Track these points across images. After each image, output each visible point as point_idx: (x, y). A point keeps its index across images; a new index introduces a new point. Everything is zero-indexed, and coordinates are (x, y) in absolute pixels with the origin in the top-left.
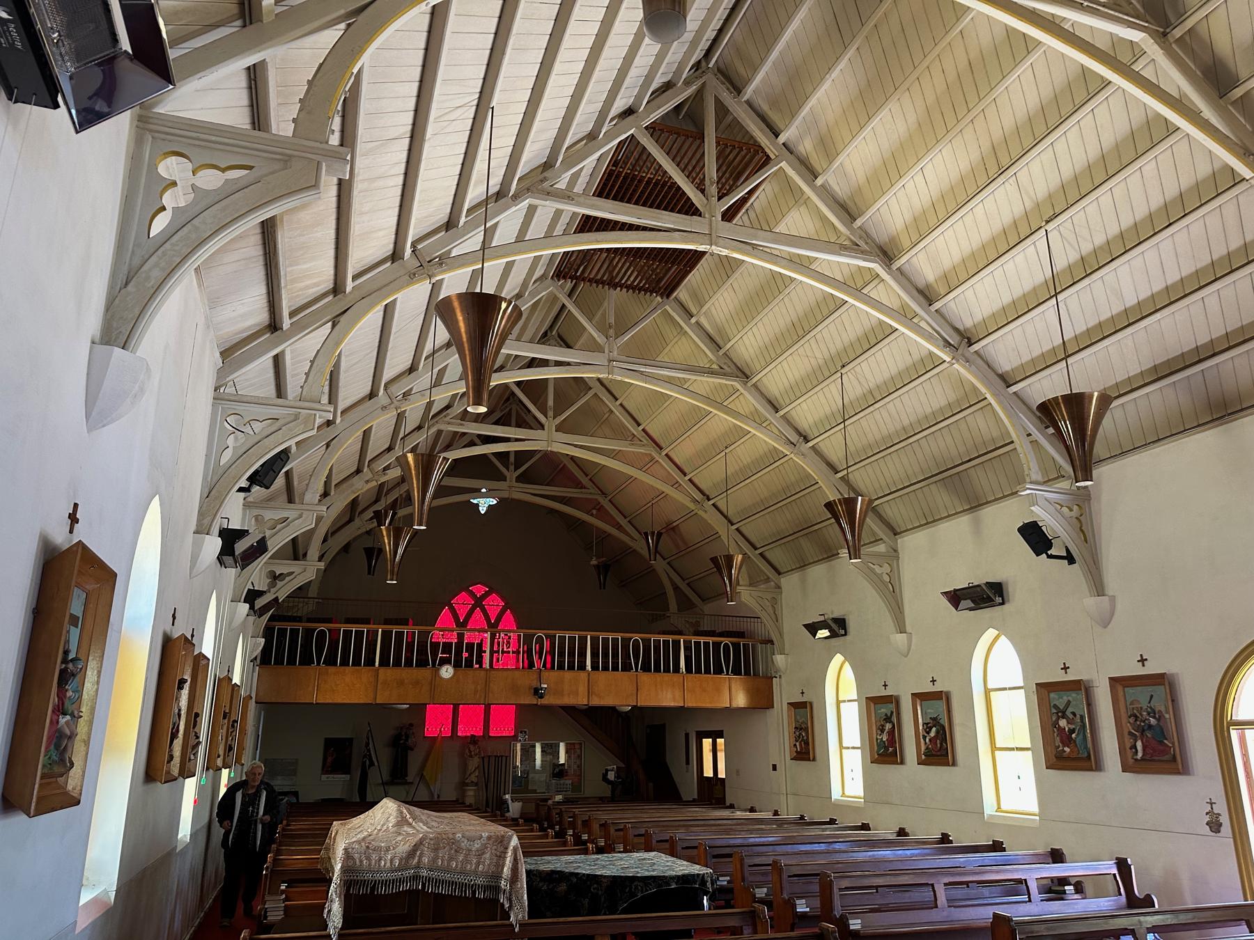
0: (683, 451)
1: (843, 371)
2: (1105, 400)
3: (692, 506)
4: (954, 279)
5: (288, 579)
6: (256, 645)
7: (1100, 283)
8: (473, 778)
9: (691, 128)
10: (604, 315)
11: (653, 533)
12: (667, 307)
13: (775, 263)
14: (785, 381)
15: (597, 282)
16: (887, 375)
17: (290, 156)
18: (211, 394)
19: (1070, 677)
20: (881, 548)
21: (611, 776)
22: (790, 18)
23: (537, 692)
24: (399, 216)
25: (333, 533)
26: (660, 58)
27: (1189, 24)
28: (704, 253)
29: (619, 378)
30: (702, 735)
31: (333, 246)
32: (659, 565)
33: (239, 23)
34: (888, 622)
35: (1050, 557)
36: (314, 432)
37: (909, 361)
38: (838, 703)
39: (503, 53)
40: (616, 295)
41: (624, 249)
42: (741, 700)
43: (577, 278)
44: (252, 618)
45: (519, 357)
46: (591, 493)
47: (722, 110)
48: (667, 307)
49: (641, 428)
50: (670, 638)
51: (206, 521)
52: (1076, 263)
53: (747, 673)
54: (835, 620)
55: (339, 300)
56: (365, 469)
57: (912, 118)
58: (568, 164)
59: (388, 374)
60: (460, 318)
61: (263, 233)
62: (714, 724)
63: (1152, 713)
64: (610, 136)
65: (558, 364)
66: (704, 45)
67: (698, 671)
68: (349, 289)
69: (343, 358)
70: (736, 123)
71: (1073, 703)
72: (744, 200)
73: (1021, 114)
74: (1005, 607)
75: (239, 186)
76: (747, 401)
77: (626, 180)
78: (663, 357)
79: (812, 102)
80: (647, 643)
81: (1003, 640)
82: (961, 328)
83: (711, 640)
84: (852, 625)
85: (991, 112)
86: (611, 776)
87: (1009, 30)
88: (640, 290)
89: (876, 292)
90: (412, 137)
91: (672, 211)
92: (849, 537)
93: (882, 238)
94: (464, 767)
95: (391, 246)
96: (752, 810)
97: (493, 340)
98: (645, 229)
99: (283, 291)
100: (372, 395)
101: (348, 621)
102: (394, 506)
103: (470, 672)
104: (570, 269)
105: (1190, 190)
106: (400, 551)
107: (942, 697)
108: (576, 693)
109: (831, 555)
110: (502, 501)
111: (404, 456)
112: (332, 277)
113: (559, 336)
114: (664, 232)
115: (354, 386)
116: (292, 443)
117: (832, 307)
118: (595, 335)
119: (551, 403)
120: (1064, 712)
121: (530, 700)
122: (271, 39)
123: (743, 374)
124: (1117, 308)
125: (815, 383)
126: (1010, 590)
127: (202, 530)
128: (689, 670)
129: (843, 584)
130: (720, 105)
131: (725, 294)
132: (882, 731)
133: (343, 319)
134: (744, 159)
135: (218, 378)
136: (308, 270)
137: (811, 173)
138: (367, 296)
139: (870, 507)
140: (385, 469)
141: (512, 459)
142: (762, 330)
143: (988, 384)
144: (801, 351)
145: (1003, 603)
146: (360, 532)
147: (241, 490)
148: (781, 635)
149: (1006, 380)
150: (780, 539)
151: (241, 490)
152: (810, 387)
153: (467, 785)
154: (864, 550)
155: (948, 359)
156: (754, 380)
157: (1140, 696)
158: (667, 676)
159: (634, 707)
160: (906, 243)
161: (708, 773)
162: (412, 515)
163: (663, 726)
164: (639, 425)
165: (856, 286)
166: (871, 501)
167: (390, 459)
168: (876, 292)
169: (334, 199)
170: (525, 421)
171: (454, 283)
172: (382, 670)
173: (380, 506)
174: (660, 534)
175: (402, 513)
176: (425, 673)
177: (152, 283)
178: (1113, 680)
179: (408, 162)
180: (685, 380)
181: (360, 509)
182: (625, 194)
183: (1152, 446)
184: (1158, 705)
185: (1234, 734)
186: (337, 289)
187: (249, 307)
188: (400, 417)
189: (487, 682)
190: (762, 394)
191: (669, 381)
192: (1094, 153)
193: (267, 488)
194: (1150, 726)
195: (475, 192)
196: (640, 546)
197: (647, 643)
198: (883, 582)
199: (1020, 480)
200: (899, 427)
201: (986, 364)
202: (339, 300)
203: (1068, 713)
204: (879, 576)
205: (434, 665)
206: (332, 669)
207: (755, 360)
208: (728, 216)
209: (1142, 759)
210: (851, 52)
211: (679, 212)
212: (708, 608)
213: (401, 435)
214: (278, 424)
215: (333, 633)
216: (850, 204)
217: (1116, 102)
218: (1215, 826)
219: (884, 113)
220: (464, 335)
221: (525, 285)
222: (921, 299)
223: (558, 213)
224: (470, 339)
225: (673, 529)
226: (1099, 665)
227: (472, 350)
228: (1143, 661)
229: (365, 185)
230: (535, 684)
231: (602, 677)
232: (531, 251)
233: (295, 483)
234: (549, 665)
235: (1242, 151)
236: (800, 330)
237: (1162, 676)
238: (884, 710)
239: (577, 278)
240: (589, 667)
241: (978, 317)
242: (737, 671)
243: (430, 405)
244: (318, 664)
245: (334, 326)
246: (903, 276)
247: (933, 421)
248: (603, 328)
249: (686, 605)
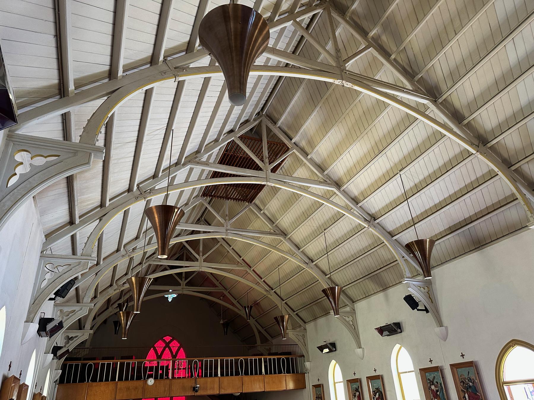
0: (260, 268)
1: (325, 232)
2: (432, 242)
3: (265, 293)
4: (366, 194)
5: (75, 339)
6: (57, 374)
7: (423, 194)
9: (257, 137)
10: (224, 210)
11: (248, 307)
12: (251, 207)
13: (294, 189)
14: (302, 236)
15: (221, 197)
16: (343, 233)
17: (77, 151)
18: (39, 254)
19: (433, 365)
20: (348, 309)
22: (293, 96)
23: (194, 389)
24: (131, 173)
25: (98, 315)
26: (243, 111)
27: (444, 97)
28: (264, 185)
29: (231, 237)
31: (100, 187)
32: (252, 321)
33: (58, 97)
34: (354, 344)
35: (418, 310)
36: (88, 270)
37: (351, 227)
38: (335, 383)
39: (177, 109)
40: (229, 202)
41: (232, 184)
42: (291, 386)
43: (212, 196)
44: (55, 361)
45: (183, 231)
47: (269, 130)
48: (251, 207)
49: (241, 258)
50: (257, 358)
51: (32, 316)
52: (413, 187)
53: (293, 372)
54: (331, 344)
55: (103, 210)
56: (114, 284)
57: (343, 133)
58: (206, 151)
59: (125, 241)
60: (156, 216)
61: (68, 182)
63: (470, 380)
64: (223, 141)
65: (204, 232)
66: (260, 106)
67: (271, 373)
68: (107, 205)
69: (104, 235)
70: (275, 135)
71: (436, 377)
72: (280, 164)
73: (385, 131)
74: (402, 333)
75: (52, 164)
76: (286, 245)
77: (231, 157)
78: (250, 228)
79: (304, 127)
80: (246, 361)
81: (403, 349)
82: (371, 213)
83: (276, 357)
84: (338, 346)
85: (374, 130)
87: (377, 100)
88: (239, 200)
89: (335, 199)
90: (137, 141)
91: (251, 169)
92: (334, 305)
93: (335, 178)
95: (128, 186)
97: (171, 225)
98: (240, 176)
99: (76, 207)
100: (118, 250)
101: (104, 359)
102: (127, 301)
103: (162, 381)
104: (207, 192)
105: (453, 158)
106: (129, 323)
107: (379, 378)
109: (327, 313)
110: (179, 295)
111: (131, 278)
112: (100, 200)
113: (205, 220)
114: (247, 177)
115: (109, 246)
116: (79, 274)
117: (318, 206)
118: (220, 219)
119: (201, 249)
120: (433, 382)
121: (191, 393)
122: (72, 103)
123: (284, 234)
124: (432, 204)
125: (314, 237)
126: (404, 326)
127: (29, 320)
128: (266, 373)
129: (332, 327)
130: (267, 127)
131: (275, 201)
132: (355, 396)
133: (104, 218)
134: (278, 149)
135: (43, 247)
136: (88, 196)
137: (306, 154)
138: (115, 208)
139: (341, 291)
140: (124, 284)
141: (184, 275)
142: (291, 215)
143: (384, 237)
144: (307, 224)
145: (401, 332)
146: (112, 314)
147: (51, 299)
149: (391, 234)
150: (304, 307)
151: (51, 299)
152: (312, 239)
154: (341, 310)
155: (367, 226)
156: (289, 236)
157: (464, 372)
158: (256, 377)
159: (241, 393)
160: (345, 180)
162: (133, 306)
164: (240, 257)
165: (327, 197)
166: (341, 288)
167: (124, 280)
168: (335, 199)
169: (101, 168)
170: (190, 258)
171: (157, 200)
172: (119, 383)
173: (121, 301)
174: (251, 307)
175: (130, 304)
176: (140, 383)
177: (6, 207)
178: (452, 366)
179: (135, 152)
180: (260, 237)
181: (111, 303)
182: (231, 162)
183: (453, 260)
184: (472, 376)
185: (506, 388)
186: (102, 205)
187: (59, 214)
188: (131, 259)
189: (170, 386)
190: (292, 242)
191: (253, 238)
192: (415, 145)
193: (63, 298)
194: (470, 386)
195: (165, 164)
196: (242, 313)
199: (402, 277)
200: (350, 255)
201: (382, 228)
202: (103, 210)
203: (434, 382)
204: (348, 322)
205: (144, 379)
206: (94, 384)
207: (289, 228)
208: (274, 170)
210: (318, 109)
211: (254, 169)
212: (275, 341)
213: (131, 268)
214: (71, 266)
215: (97, 365)
216: (322, 166)
217: (421, 125)
219: (332, 131)
220: (158, 224)
221: (189, 200)
222: (353, 202)
223: (203, 171)
224: (160, 225)
225: (257, 304)
226: (446, 360)
227: (161, 230)
229: (116, 161)
230: (193, 385)
231: (226, 379)
232: (191, 186)
233: (80, 293)
234: (200, 374)
235: (470, 143)
236: (306, 215)
237: (472, 362)
238: (355, 386)
239: (212, 196)
240: (219, 375)
241: (377, 209)
242: (288, 372)
243: (145, 253)
244: (88, 381)
245: (100, 221)
246: (345, 193)
247: (364, 252)
248: (224, 217)
249: (264, 340)
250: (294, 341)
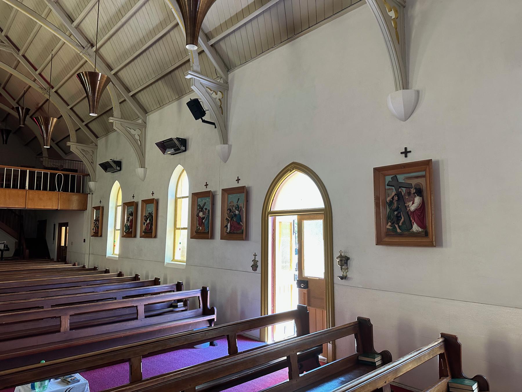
30: (61, 225)
34: (137, 164)
35: (204, 121)
53: (78, 191)
63: (238, 208)
67: (38, 188)
84: (124, 166)
120: (202, 209)
128: (31, 187)
145: (185, 151)
157: (233, 198)
158: (14, 191)
161: (63, 244)
163: (46, 221)
184: (242, 204)
185: (270, 219)
194: (235, 215)
198: (136, 140)
204: (133, 136)
209: (230, 233)
218: (255, 267)
228: (238, 180)
238: (132, 209)
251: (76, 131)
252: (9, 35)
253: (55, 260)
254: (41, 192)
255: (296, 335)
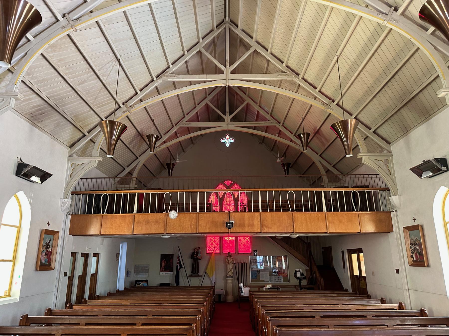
8: (231, 274)
21: (299, 275)
30: (351, 252)
42: (370, 228)
46: (271, 123)
53: (372, 210)
62: (355, 244)
86: (299, 275)
94: (226, 268)
96: (383, 301)
108: (253, 225)
113: (231, 21)
119: (227, 58)
148: (394, 183)
153: (227, 277)
161: (356, 273)
163: (331, 246)
176: (161, 216)
197: (298, 193)
230: (227, 220)
242: (364, 209)
250: (373, 170)
251: (364, 139)
252: (289, 64)
253: (350, 291)
254: (340, 213)
255: (307, 284)
